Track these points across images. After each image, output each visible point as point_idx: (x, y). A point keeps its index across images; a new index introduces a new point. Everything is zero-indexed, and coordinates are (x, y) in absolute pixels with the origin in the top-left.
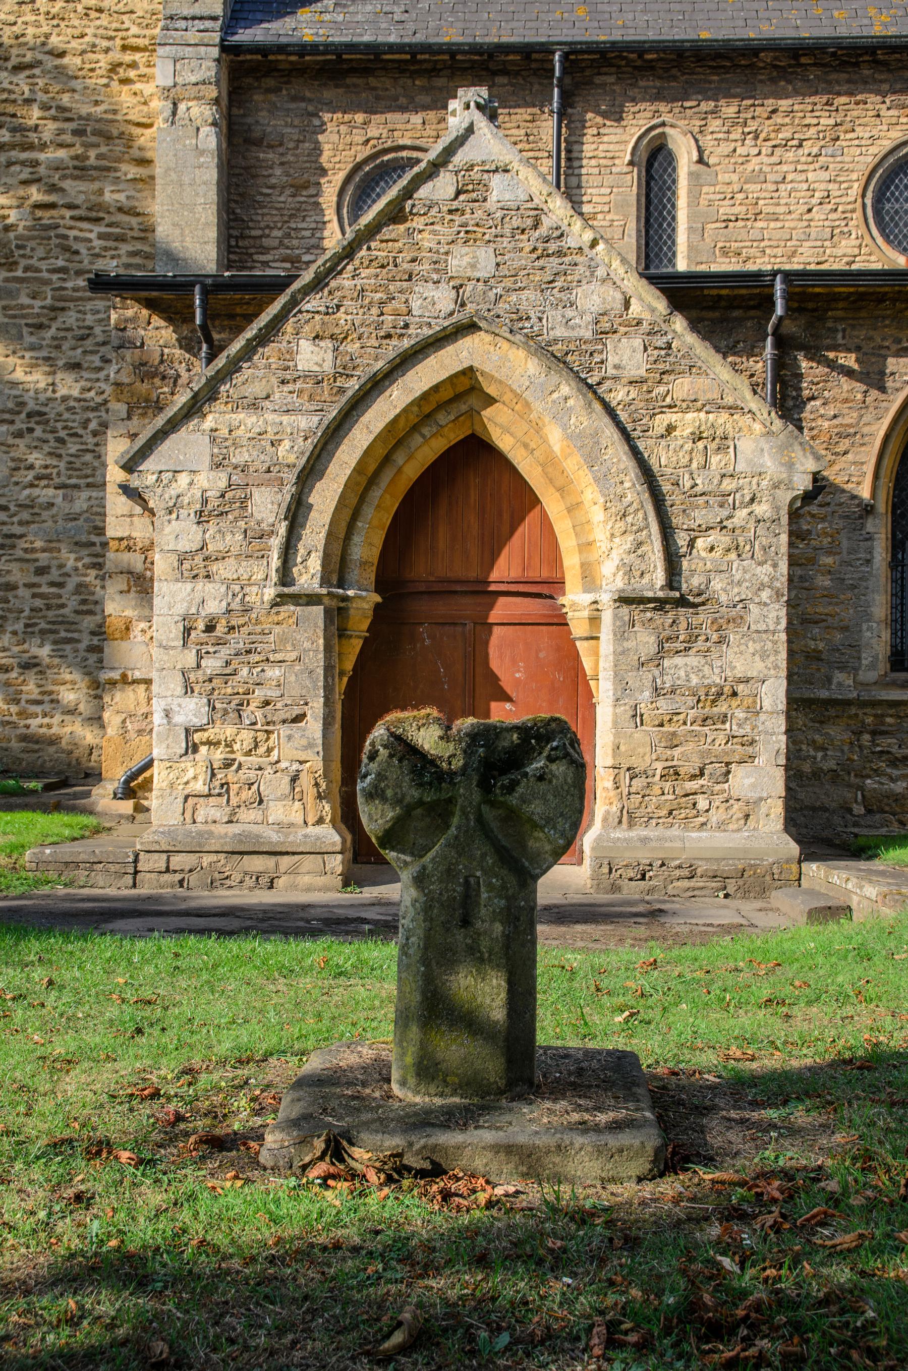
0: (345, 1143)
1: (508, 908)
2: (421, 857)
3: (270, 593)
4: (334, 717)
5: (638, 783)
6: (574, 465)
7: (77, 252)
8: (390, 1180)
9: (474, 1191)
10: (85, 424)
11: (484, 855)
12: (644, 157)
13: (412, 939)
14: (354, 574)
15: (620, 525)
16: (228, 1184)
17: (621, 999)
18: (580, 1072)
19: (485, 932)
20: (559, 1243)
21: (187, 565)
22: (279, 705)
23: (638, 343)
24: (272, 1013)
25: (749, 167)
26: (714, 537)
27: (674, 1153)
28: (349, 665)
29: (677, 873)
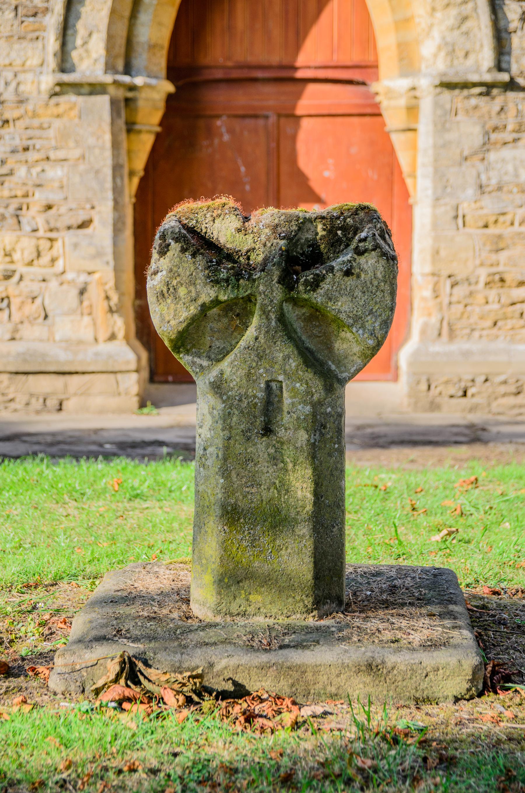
0: (140, 665)
1: (314, 414)
2: (219, 361)
3: (48, 80)
4: (124, 223)
5: (460, 292)
8: (189, 701)
9: (279, 712)
11: (286, 358)
13: (210, 450)
14: (140, 60)
16: (16, 709)
17: (439, 519)
18: (393, 589)
20: (369, 762)
22: (63, 210)
24: (62, 537)
27: (494, 672)
28: (140, 163)
29: (503, 389)
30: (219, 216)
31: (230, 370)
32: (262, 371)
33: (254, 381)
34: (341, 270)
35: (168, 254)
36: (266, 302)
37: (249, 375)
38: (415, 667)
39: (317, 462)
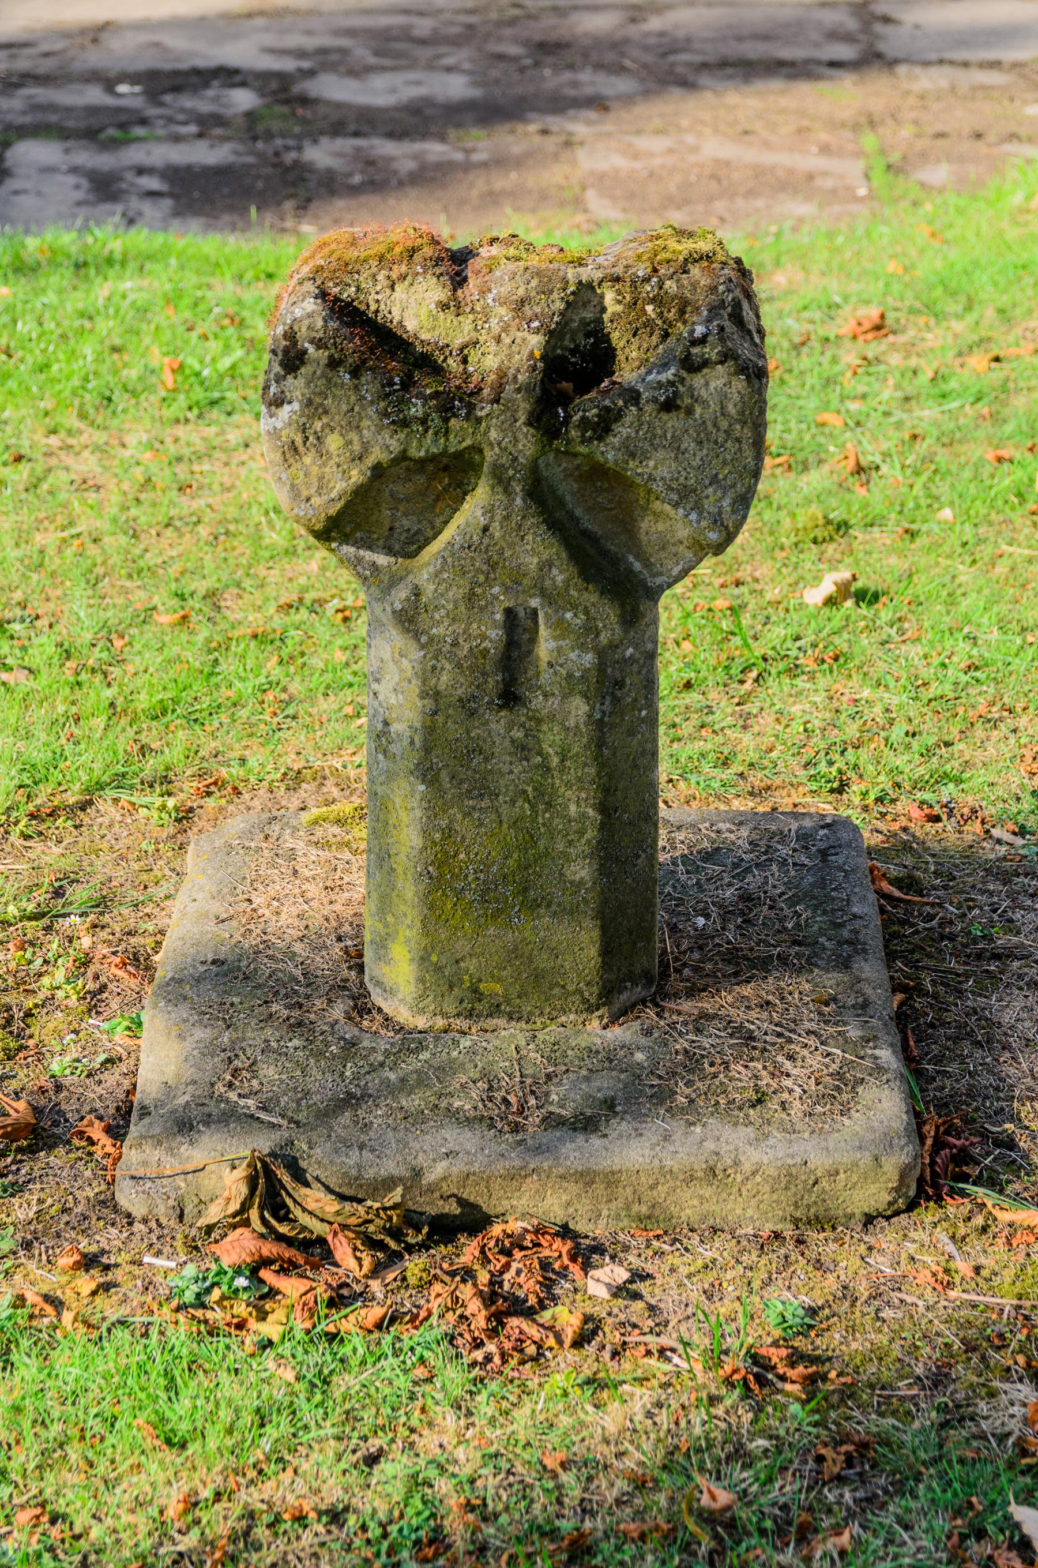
0: (286, 1178)
1: (601, 667)
19: (552, 717)
30: (403, 277)
31: (432, 587)
32: (496, 590)
33: (482, 609)
34: (655, 400)
35: (303, 370)
36: (504, 460)
37: (471, 598)
38: (794, 1171)
39: (606, 752)
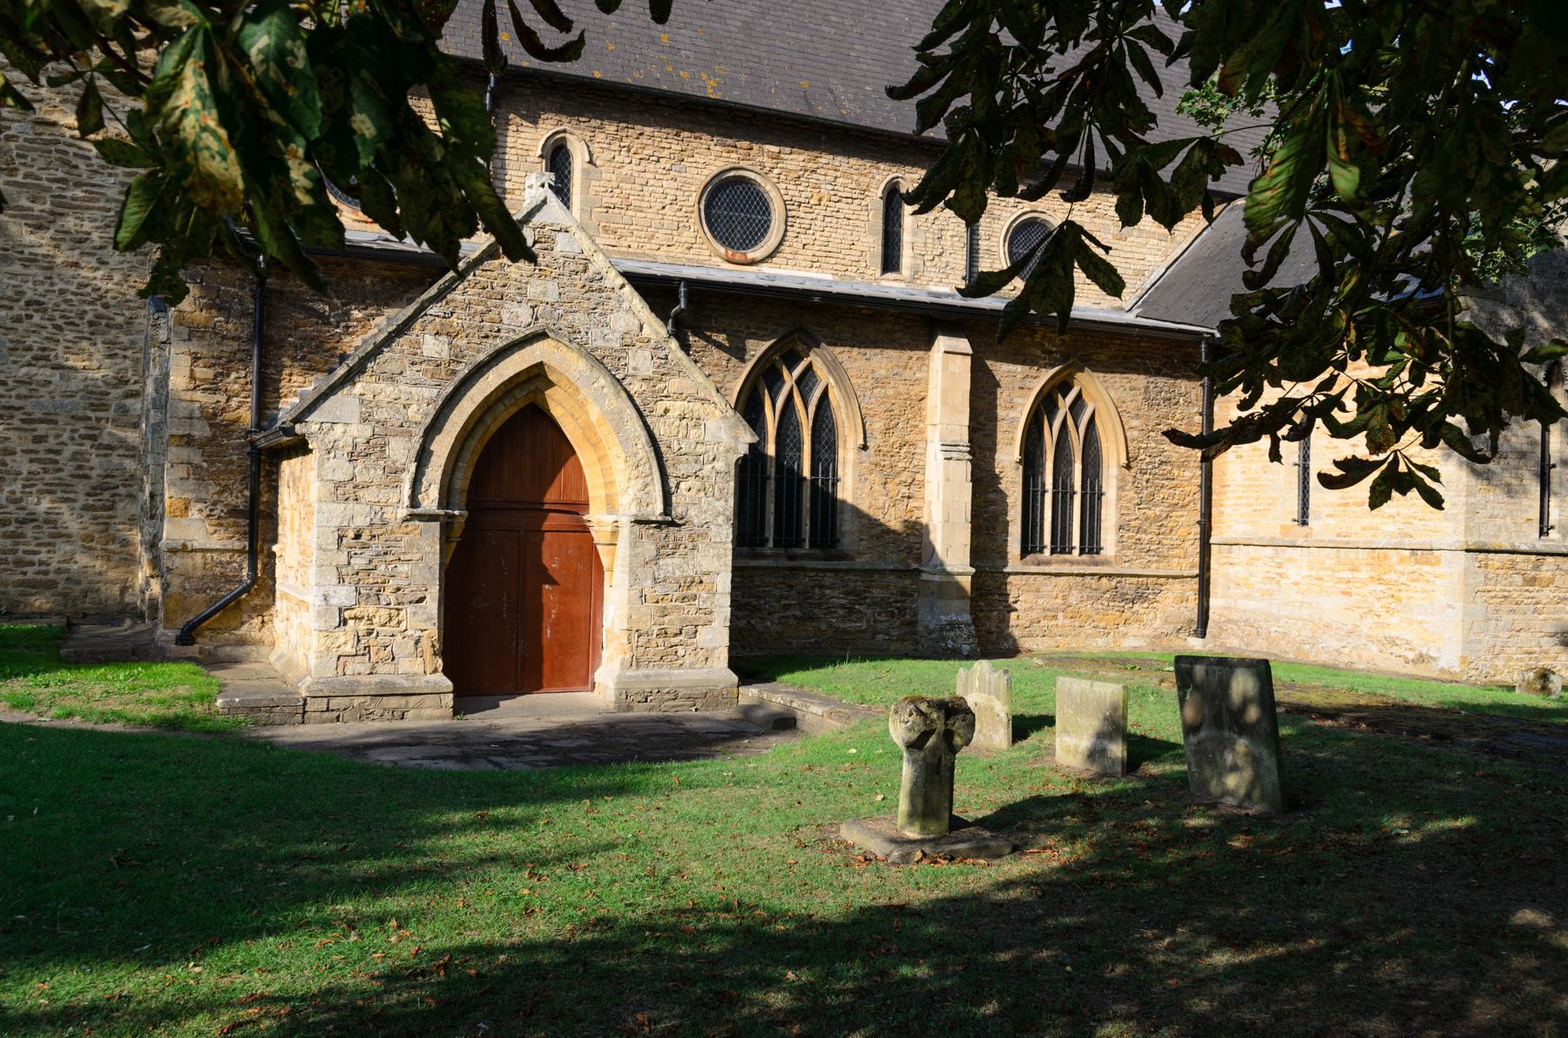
3: (403, 512)
5: (643, 640)
6: (605, 432)
7: (76, 167)
10: (82, 314)
12: (549, 150)
15: (635, 473)
21: (340, 491)
23: (648, 354)
25: (624, 171)
26: (691, 482)
